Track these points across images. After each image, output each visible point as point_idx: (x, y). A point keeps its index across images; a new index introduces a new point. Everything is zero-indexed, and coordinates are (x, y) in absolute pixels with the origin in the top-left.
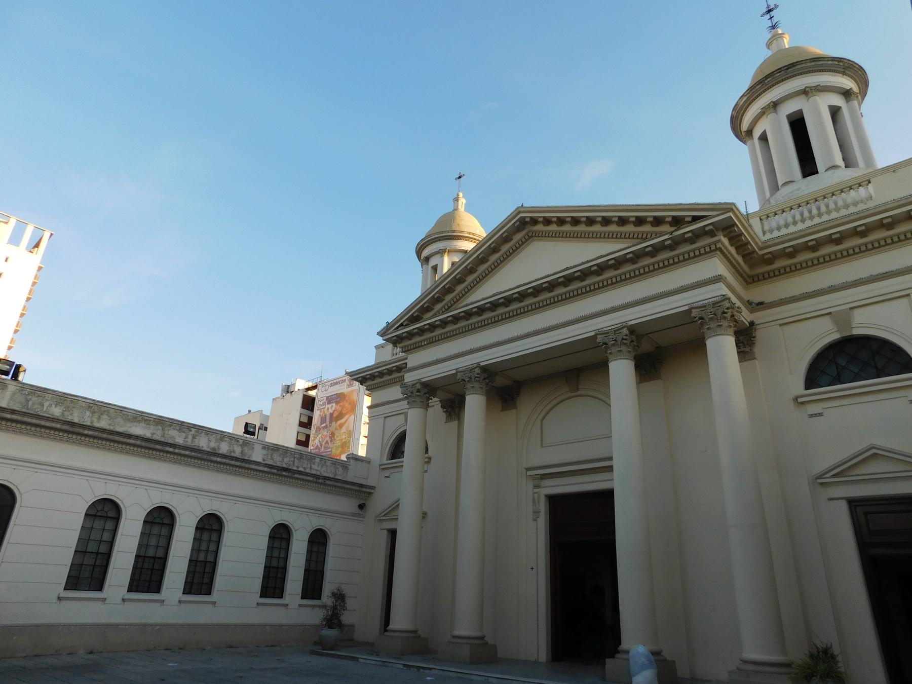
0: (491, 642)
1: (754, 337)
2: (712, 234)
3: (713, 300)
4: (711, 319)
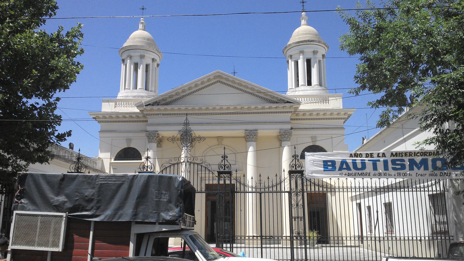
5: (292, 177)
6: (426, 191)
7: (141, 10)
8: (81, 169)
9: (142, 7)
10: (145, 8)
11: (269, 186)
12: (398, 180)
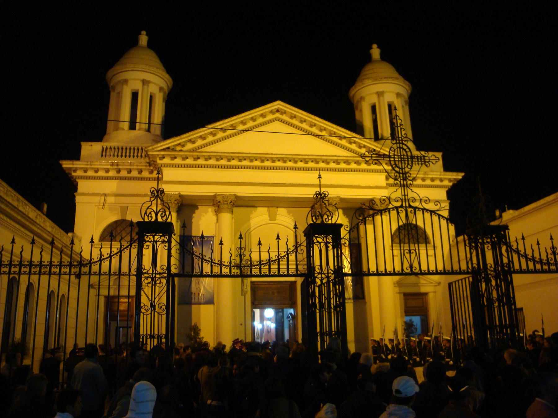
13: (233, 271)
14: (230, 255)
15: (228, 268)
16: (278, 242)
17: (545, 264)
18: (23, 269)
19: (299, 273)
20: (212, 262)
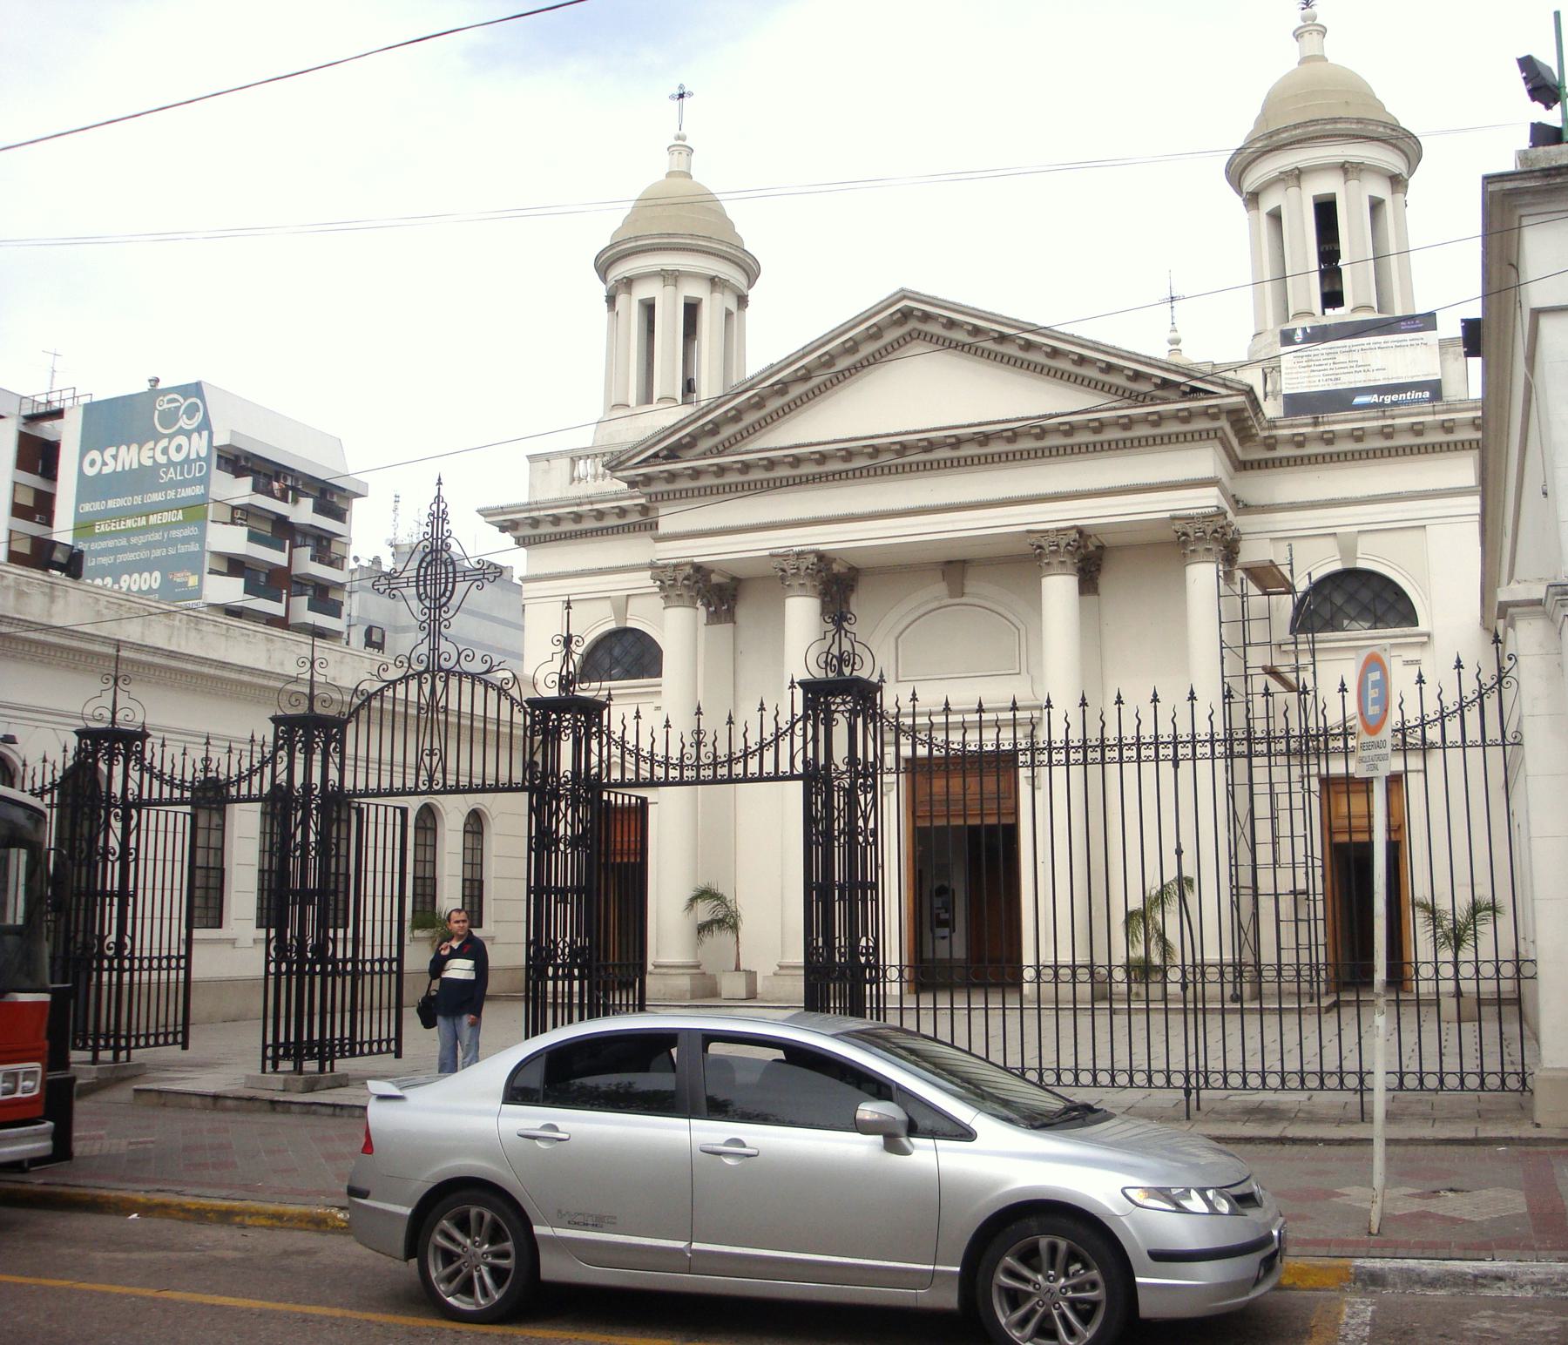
0: (709, 972)
1: (1237, 553)
2: (1215, 417)
3: (1203, 510)
4: (1199, 539)
5: (836, 711)
6: (674, 768)
7: (676, 103)
8: (854, 663)
9: (677, 92)
10: (686, 90)
11: (1403, 724)
12: (318, 751)
13: (686, 773)
14: (1101, 724)
15: (1208, 744)
16: (1459, 674)
17: (923, 743)
18: (1243, 748)
19: (795, 772)
20: (171, 783)
